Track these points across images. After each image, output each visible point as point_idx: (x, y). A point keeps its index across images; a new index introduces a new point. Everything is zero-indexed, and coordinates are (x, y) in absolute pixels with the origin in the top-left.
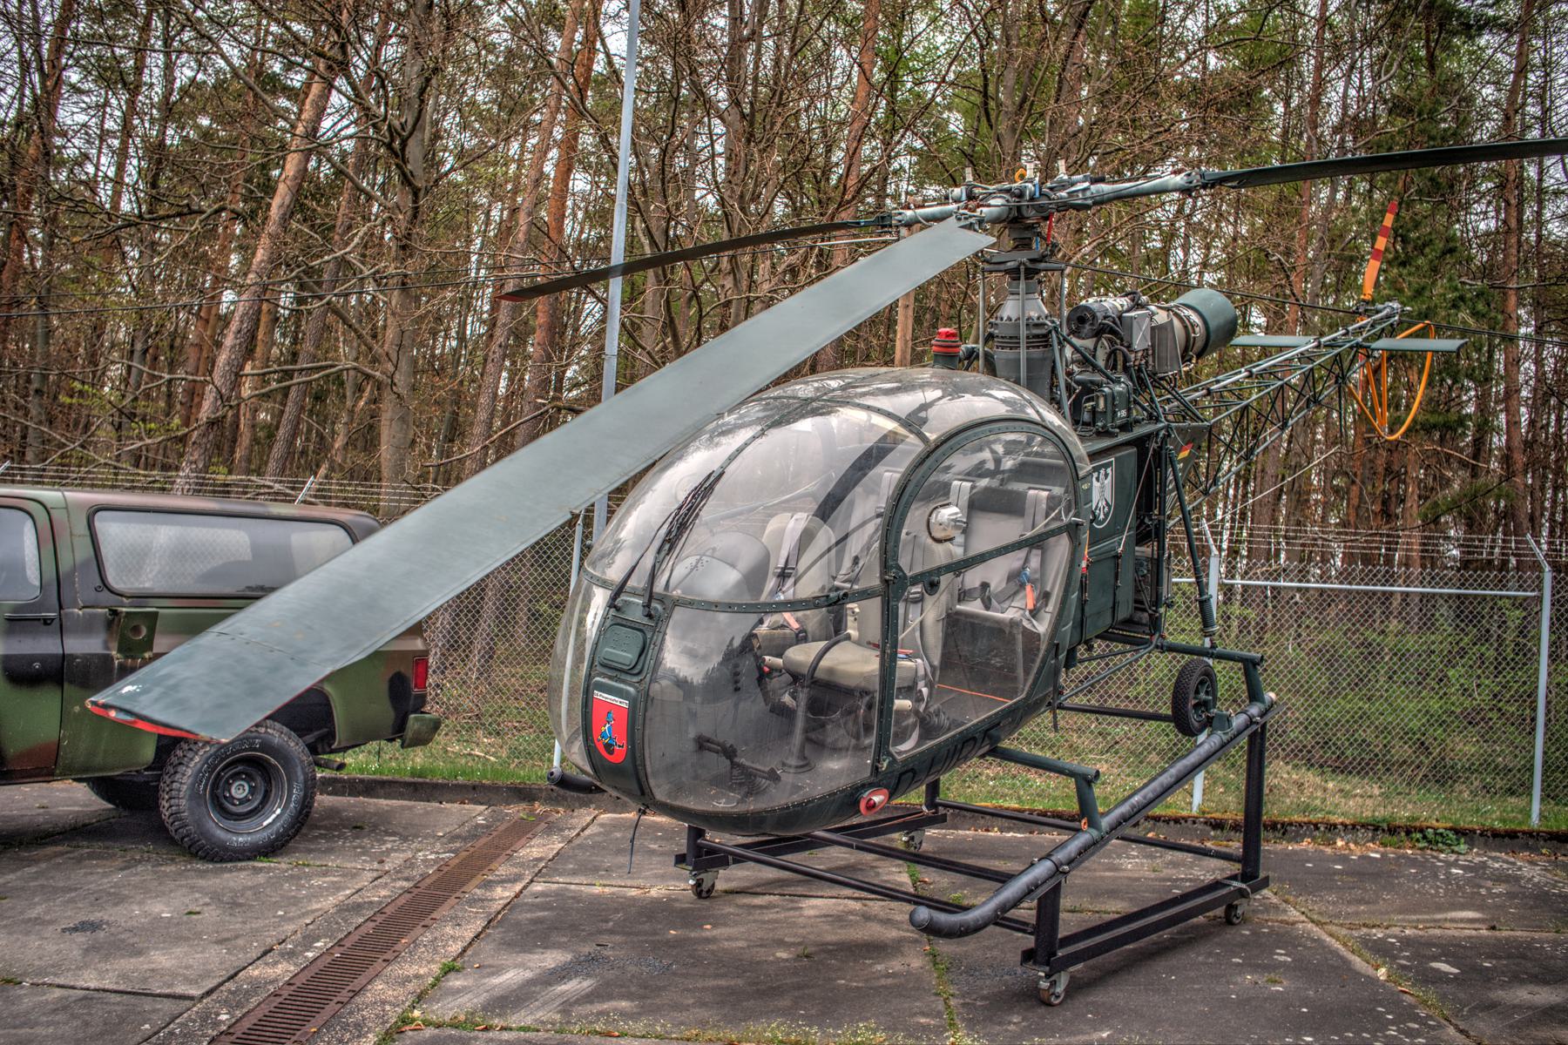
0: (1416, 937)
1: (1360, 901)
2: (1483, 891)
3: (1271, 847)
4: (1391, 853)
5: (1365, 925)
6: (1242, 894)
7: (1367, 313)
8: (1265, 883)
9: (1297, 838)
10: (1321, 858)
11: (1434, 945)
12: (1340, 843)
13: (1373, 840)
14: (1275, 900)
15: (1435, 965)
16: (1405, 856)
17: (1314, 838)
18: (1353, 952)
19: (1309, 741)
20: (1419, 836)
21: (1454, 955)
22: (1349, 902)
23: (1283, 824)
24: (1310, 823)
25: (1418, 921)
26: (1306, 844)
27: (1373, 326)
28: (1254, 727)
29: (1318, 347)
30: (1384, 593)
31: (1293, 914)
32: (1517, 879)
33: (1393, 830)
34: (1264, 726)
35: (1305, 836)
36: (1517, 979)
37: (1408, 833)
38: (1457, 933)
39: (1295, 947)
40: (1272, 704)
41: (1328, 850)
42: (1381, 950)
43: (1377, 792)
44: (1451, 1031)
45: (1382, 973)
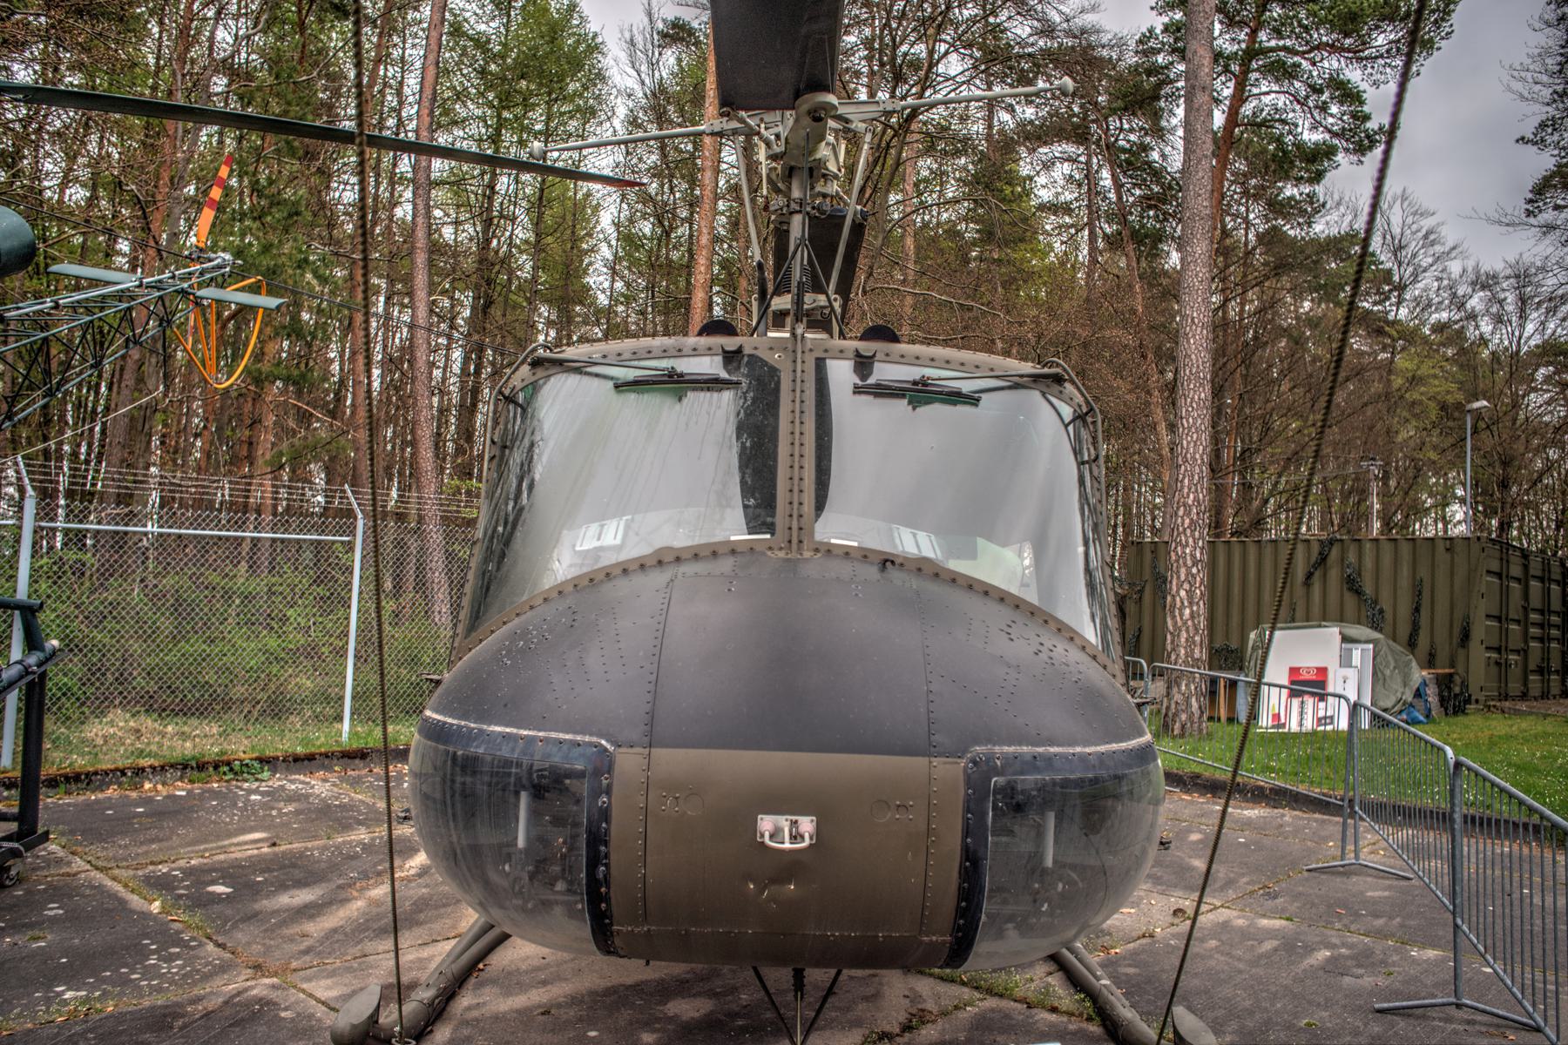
0: (201, 864)
1: (152, 841)
2: (274, 813)
3: (49, 801)
4: (197, 788)
5: (152, 863)
6: (15, 854)
7: (199, 260)
8: (45, 837)
9: (101, 788)
10: (127, 803)
11: (215, 870)
12: (147, 786)
13: (181, 779)
14: (61, 853)
15: (211, 889)
16: (211, 791)
17: (120, 785)
18: (133, 891)
19: (152, 687)
20: (226, 769)
21: (231, 876)
22: (142, 843)
23: (87, 774)
24: (117, 769)
25: (206, 850)
26: (112, 792)
27: (202, 274)
28: (30, 677)
29: (140, 286)
30: (236, 538)
31: (78, 864)
32: (307, 796)
33: (201, 767)
34: (43, 676)
35: (111, 783)
36: (283, 887)
37: (216, 767)
38: (238, 855)
39: (70, 897)
40: (54, 653)
41: (134, 795)
42: (162, 885)
43: (215, 731)
44: (210, 947)
45: (156, 907)
